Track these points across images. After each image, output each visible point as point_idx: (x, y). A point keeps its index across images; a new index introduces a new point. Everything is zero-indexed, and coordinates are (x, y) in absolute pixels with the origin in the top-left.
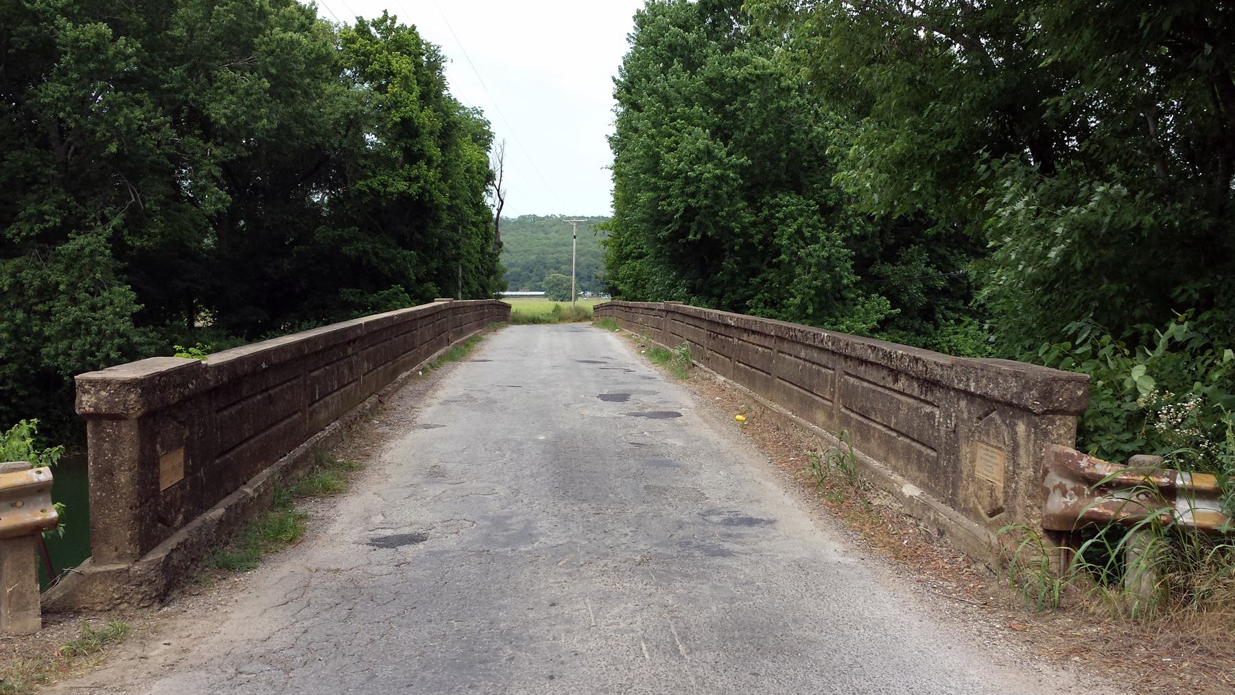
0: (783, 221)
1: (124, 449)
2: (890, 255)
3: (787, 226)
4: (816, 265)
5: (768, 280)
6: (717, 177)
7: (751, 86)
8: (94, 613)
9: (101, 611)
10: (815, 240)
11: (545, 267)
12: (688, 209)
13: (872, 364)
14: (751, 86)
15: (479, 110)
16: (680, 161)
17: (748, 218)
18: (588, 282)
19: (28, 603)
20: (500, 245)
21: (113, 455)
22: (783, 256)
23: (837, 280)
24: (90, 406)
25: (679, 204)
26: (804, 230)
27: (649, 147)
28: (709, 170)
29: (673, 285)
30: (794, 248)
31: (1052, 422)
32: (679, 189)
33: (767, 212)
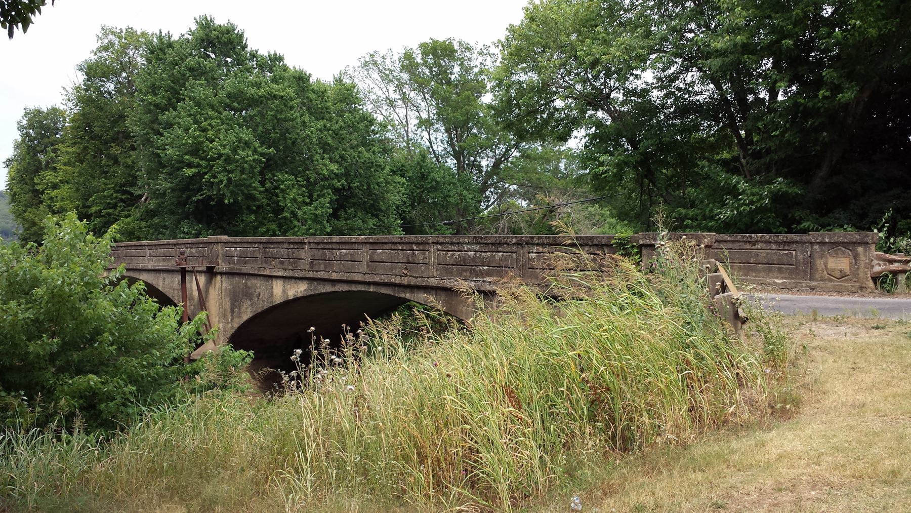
4: (311, 219)
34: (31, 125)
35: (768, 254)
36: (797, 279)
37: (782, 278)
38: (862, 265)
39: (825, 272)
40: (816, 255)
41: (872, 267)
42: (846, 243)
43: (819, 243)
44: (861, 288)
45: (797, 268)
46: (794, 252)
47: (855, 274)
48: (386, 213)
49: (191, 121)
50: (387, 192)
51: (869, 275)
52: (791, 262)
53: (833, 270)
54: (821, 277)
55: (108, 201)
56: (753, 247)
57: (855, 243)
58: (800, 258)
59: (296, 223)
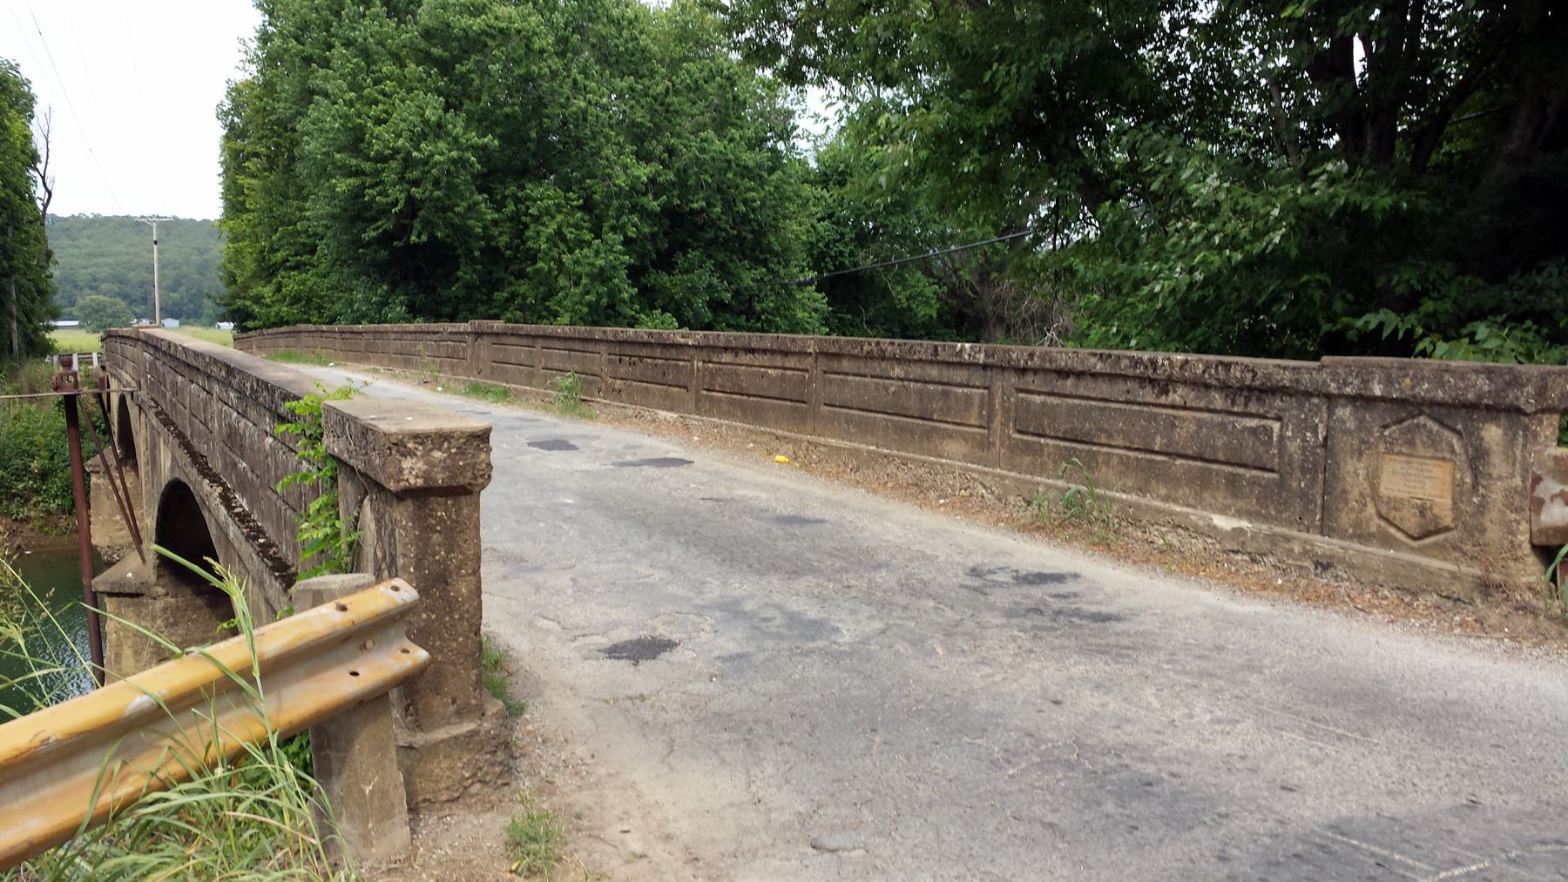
0: (537, 219)
1: (465, 541)
2: (665, 262)
3: (543, 224)
4: (588, 275)
5: (518, 295)
6: (454, 161)
7: (490, 43)
8: (438, 805)
9: (448, 801)
10: (581, 243)
11: (76, 287)
12: (410, 199)
13: (1102, 375)
14: (490, 43)
15: (13, 63)
16: (399, 136)
17: (491, 215)
18: (143, 307)
19: (392, 805)
20: (49, 254)
21: (448, 553)
22: (540, 264)
23: (612, 294)
24: (417, 477)
25: (397, 193)
26: (565, 230)
27: (346, 117)
28: (440, 152)
29: (384, 303)
30: (555, 253)
31: (1540, 423)
32: (397, 174)
33: (513, 208)
34: (237, 108)
35: (1200, 424)
36: (1281, 522)
37: (1239, 514)
38: (1497, 496)
39: (1371, 509)
40: (1342, 443)
41: (1538, 504)
42: (1441, 404)
43: (1353, 399)
44: (1485, 587)
45: (1281, 484)
46: (1276, 426)
47: (1474, 530)
48: (784, 256)
49: (345, 86)
50: (785, 217)
51: (1523, 538)
52: (1265, 461)
53: (1396, 504)
54: (1357, 524)
55: (302, 240)
56: (1163, 400)
57: (1473, 407)
58: (1293, 446)
59: (562, 281)
